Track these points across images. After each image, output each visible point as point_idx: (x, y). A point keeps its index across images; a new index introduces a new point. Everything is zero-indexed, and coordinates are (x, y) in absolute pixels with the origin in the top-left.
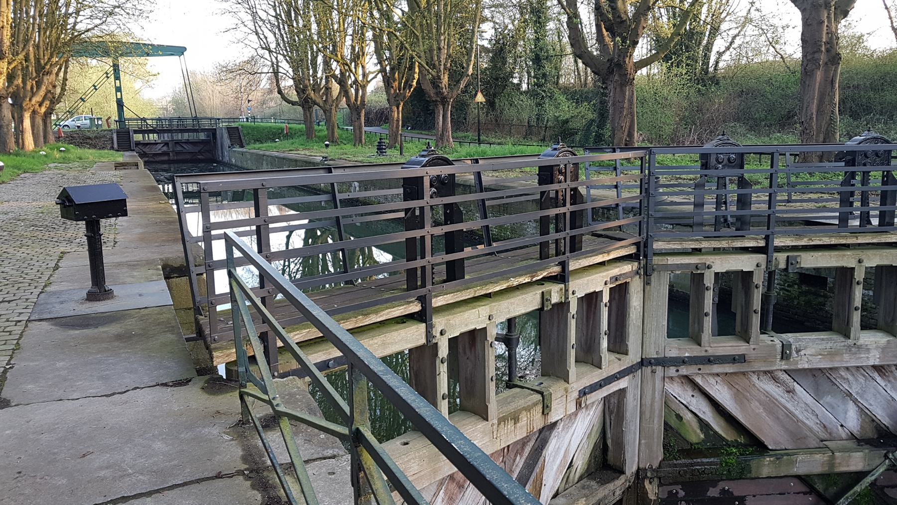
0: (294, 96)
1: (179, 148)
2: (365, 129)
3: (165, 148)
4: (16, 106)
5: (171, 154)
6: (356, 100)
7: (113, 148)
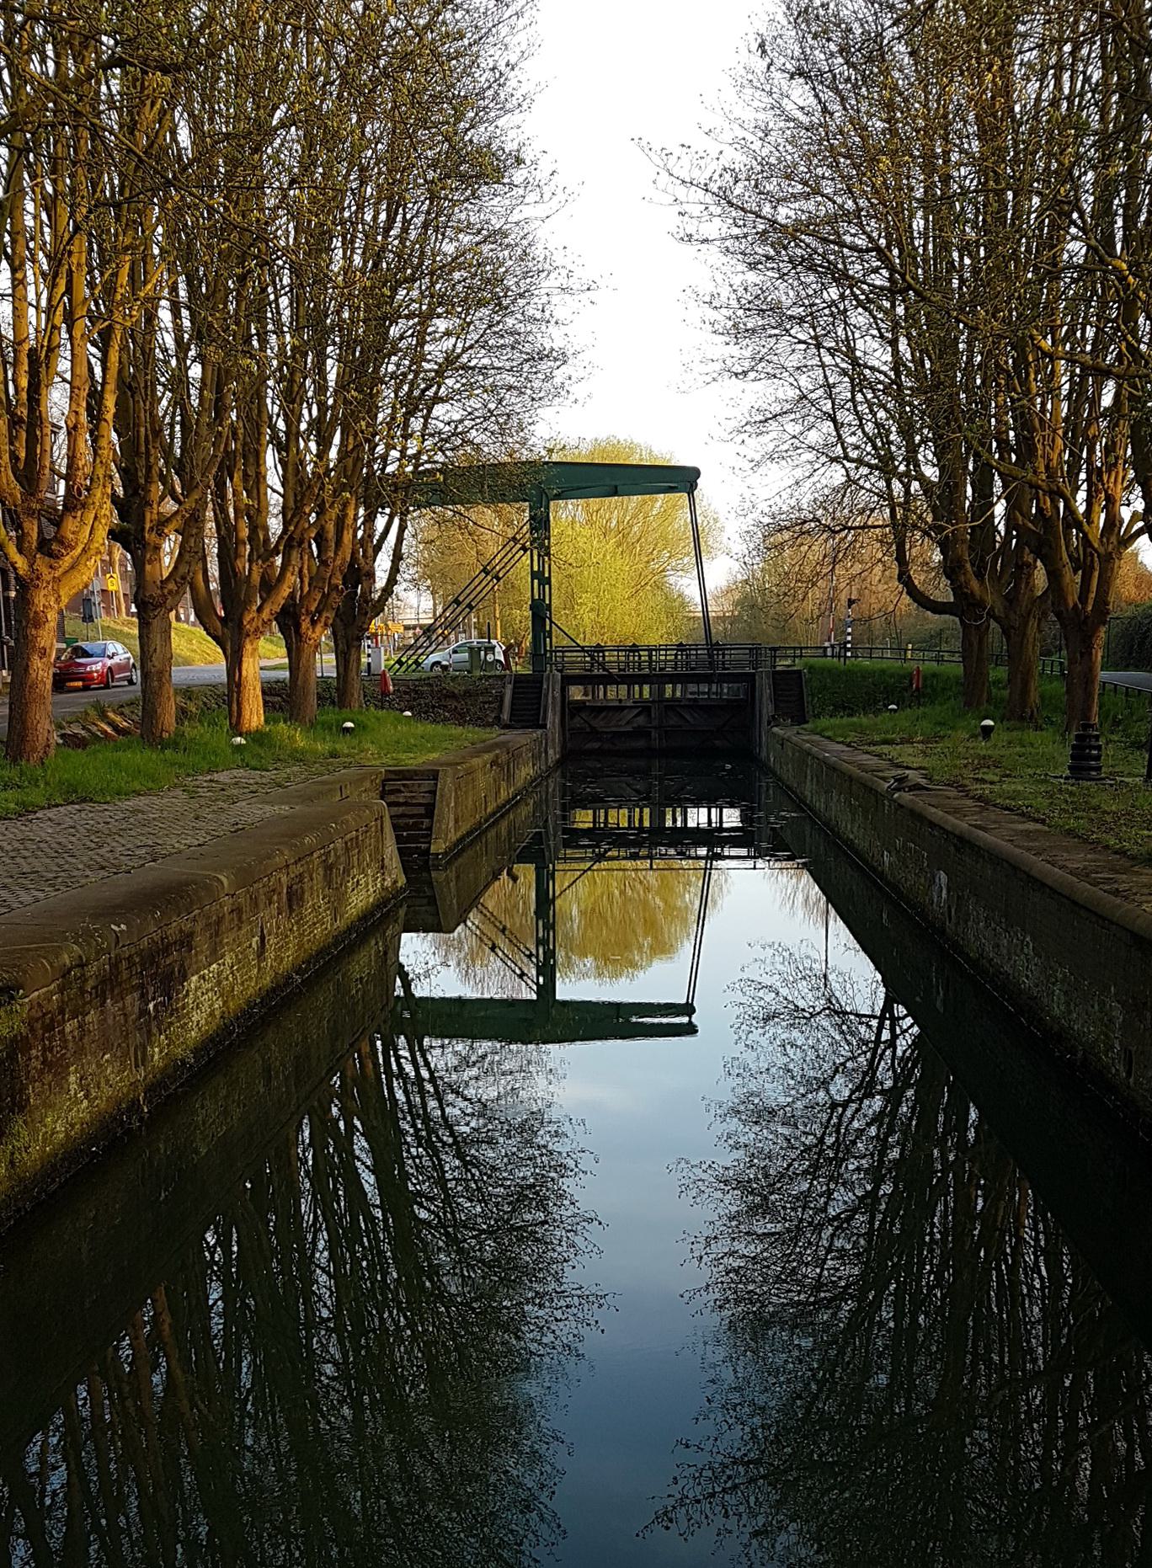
0: (943, 592)
1: (673, 720)
2: (1103, 675)
3: (641, 720)
4: (230, 624)
5: (654, 734)
6: (1083, 597)
7: (498, 718)
